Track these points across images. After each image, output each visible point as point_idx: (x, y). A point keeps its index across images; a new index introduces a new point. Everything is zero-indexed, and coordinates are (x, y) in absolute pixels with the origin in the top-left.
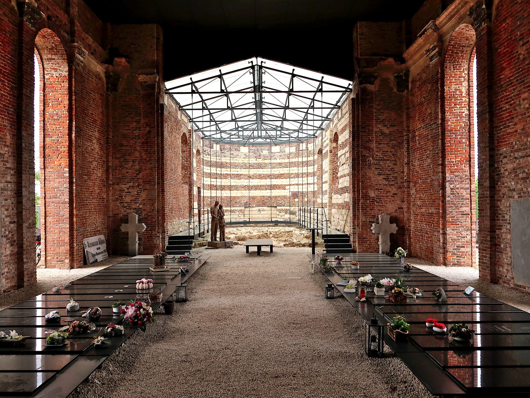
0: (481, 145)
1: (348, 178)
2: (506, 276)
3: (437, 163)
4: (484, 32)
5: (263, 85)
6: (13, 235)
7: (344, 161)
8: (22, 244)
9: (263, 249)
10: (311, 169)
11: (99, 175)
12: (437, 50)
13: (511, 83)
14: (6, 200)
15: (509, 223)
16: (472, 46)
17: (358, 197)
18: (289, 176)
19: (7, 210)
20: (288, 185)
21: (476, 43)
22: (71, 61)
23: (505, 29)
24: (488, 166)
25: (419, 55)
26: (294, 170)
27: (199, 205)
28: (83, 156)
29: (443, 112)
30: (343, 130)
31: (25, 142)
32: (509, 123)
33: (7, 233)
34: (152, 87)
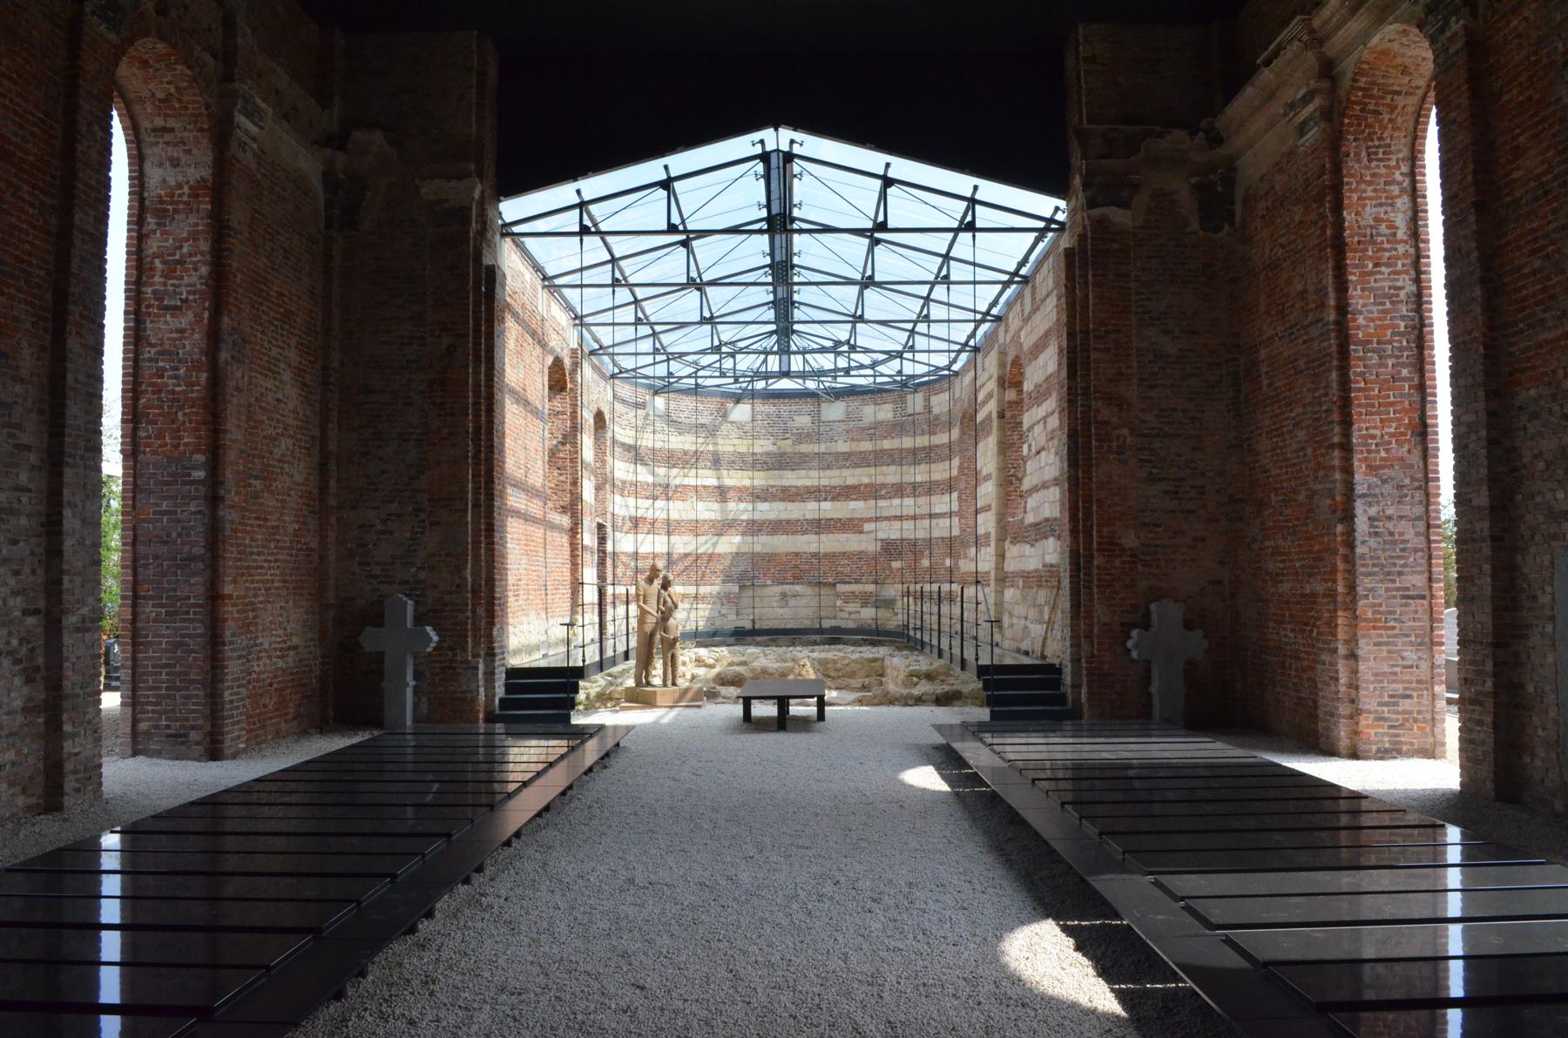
0: (1462, 382)
1: (1054, 493)
2: (1542, 781)
3: (1326, 439)
4: (1458, 45)
5: (796, 213)
7: (1042, 441)
8: (60, 678)
9: (796, 709)
10: (940, 471)
11: (299, 478)
12: (1317, 102)
13: (1546, 193)
14: (14, 542)
15: (1552, 618)
16: (1420, 92)
17: (1088, 546)
18: (872, 492)
19: (16, 573)
20: (869, 520)
21: (1435, 77)
22: (222, 135)
23: (1520, 36)
24: (1484, 443)
25: (1266, 124)
26: (890, 475)
27: (602, 577)
28: (249, 419)
29: (1342, 287)
30: (1038, 349)
32: (1544, 311)
33: (15, 642)
34: (460, 215)
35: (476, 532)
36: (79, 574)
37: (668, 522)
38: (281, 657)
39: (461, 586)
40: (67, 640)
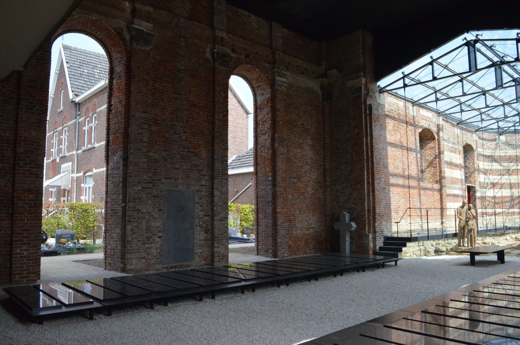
0: (225, 141)
6: (207, 225)
14: (201, 199)
19: (201, 206)
22: (272, 84)
31: (218, 155)
33: (201, 223)
35: (369, 192)
36: (220, 206)
37: (510, 184)
38: (307, 230)
39: (364, 209)
40: (215, 223)
